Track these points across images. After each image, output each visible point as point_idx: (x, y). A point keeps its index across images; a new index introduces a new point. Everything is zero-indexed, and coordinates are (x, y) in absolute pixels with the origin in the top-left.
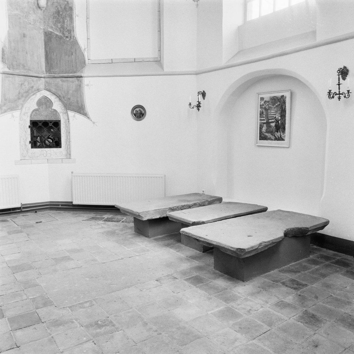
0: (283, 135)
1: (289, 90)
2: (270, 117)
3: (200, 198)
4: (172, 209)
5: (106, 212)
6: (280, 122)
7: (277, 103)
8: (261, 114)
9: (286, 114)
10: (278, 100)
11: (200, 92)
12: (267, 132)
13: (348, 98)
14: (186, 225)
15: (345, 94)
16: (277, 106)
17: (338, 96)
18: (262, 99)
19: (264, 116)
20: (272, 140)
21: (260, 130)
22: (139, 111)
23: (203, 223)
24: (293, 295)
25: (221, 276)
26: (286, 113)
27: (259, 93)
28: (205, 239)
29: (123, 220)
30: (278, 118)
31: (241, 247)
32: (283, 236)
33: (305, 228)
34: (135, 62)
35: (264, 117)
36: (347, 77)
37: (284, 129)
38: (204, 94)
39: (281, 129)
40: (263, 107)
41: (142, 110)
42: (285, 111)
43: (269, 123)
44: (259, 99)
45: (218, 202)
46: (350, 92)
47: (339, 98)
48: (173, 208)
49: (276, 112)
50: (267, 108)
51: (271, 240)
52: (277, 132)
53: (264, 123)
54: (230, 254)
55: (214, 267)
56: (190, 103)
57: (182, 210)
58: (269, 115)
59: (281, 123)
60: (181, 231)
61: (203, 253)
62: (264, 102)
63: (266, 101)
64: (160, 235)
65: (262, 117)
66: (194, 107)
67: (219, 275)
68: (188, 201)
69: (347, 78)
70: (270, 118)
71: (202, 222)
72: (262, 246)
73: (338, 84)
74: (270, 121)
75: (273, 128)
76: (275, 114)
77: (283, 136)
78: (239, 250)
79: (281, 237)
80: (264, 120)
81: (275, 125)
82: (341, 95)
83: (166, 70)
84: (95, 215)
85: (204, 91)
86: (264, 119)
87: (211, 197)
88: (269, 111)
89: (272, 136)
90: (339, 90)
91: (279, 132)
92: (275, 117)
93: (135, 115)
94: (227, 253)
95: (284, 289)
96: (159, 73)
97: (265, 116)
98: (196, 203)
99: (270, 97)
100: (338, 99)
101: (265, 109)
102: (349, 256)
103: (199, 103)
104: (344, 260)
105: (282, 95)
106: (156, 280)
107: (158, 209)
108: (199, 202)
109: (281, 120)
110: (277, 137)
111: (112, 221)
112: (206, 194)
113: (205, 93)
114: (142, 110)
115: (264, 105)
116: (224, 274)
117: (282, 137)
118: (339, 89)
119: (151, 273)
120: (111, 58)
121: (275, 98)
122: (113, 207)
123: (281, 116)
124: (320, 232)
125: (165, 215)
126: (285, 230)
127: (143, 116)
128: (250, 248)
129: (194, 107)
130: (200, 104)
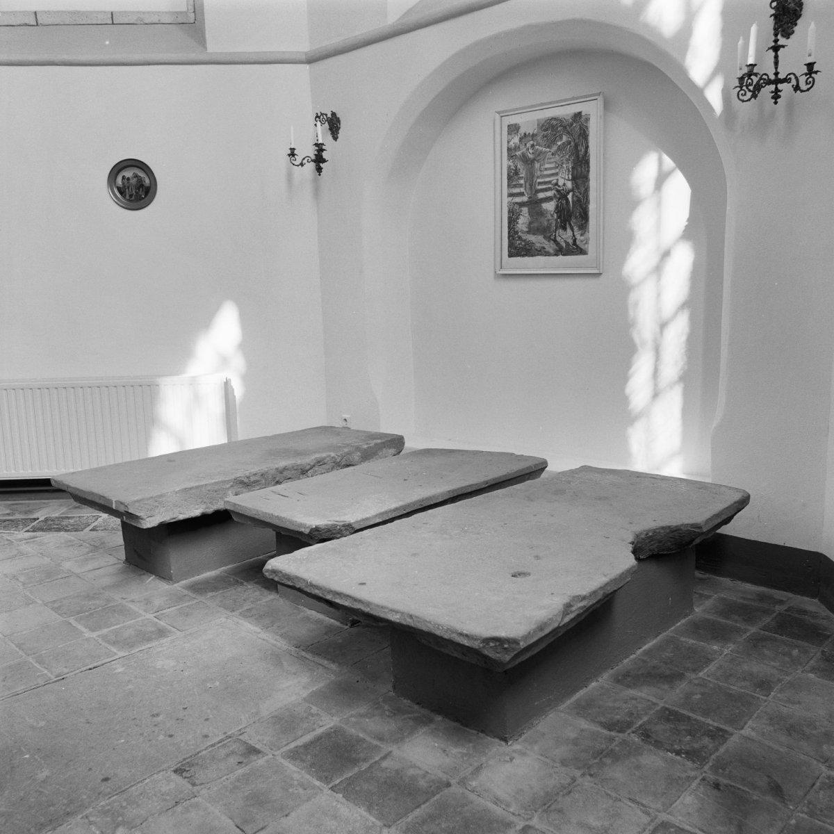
0: (582, 238)
1: (599, 94)
2: (540, 183)
3: (335, 440)
4: (246, 484)
5: (48, 499)
6: (570, 197)
7: (561, 138)
8: (513, 176)
9: (588, 171)
10: (565, 127)
11: (322, 114)
12: (531, 231)
13: (808, 89)
14: (291, 540)
15: (796, 78)
16: (559, 149)
17: (772, 87)
18: (513, 129)
19: (522, 182)
20: (547, 254)
21: (509, 227)
22: (135, 179)
23: (351, 529)
24: (694, 785)
25: (422, 721)
26: (589, 167)
27: (503, 112)
28: (356, 600)
29: (96, 524)
30: (564, 185)
31: (502, 634)
32: (633, 567)
33: (692, 525)
34: (113, 24)
35: (521, 186)
36: (796, 25)
37: (585, 216)
38: (334, 124)
39: (576, 218)
40: (518, 153)
41: (142, 174)
42: (587, 163)
43: (536, 203)
44: (505, 129)
45: (393, 451)
46: (816, 68)
47: (776, 96)
48: (246, 480)
49: (559, 166)
50: (531, 156)
51: (601, 588)
52: (564, 229)
53: (522, 204)
54: (456, 655)
55: (394, 687)
56: (292, 150)
57: (278, 483)
58: (538, 177)
59: (573, 202)
60: (268, 571)
61: (351, 627)
62: (521, 140)
63: (525, 134)
64: (209, 569)
65: (515, 186)
66: (305, 161)
67: (415, 719)
68: (298, 453)
69: (796, 29)
70: (540, 187)
71: (344, 526)
72: (572, 612)
73: (771, 48)
74: (541, 195)
75: (550, 217)
76: (557, 174)
77: (582, 241)
78: (492, 644)
79: (628, 571)
80: (521, 194)
81: (557, 207)
82: (780, 86)
83: (214, 47)
84: (8, 512)
85: (334, 114)
86: (522, 190)
87: (373, 436)
88: (537, 165)
89: (546, 242)
90: (776, 68)
91: (569, 230)
92: (555, 181)
93: (121, 193)
94: (442, 650)
95: (652, 760)
96: (193, 56)
97: (525, 182)
98: (325, 458)
99: (538, 120)
100: (773, 98)
101: (524, 159)
102: (806, 599)
103: (320, 148)
104: (797, 616)
105: (577, 110)
106: (175, 771)
107: (197, 487)
108: (333, 454)
109: (572, 190)
110: (564, 245)
111: (59, 530)
112: (353, 428)
113: (338, 120)
114: (142, 174)
115: (519, 147)
116: (432, 711)
117: (578, 243)
118: (776, 63)
119: (161, 737)
120: (35, 10)
121: (554, 122)
122: (46, 482)
123: (574, 179)
124: (721, 531)
125: (220, 506)
126: (631, 538)
127: (146, 195)
128: (535, 631)
129: (304, 162)
130: (323, 150)
